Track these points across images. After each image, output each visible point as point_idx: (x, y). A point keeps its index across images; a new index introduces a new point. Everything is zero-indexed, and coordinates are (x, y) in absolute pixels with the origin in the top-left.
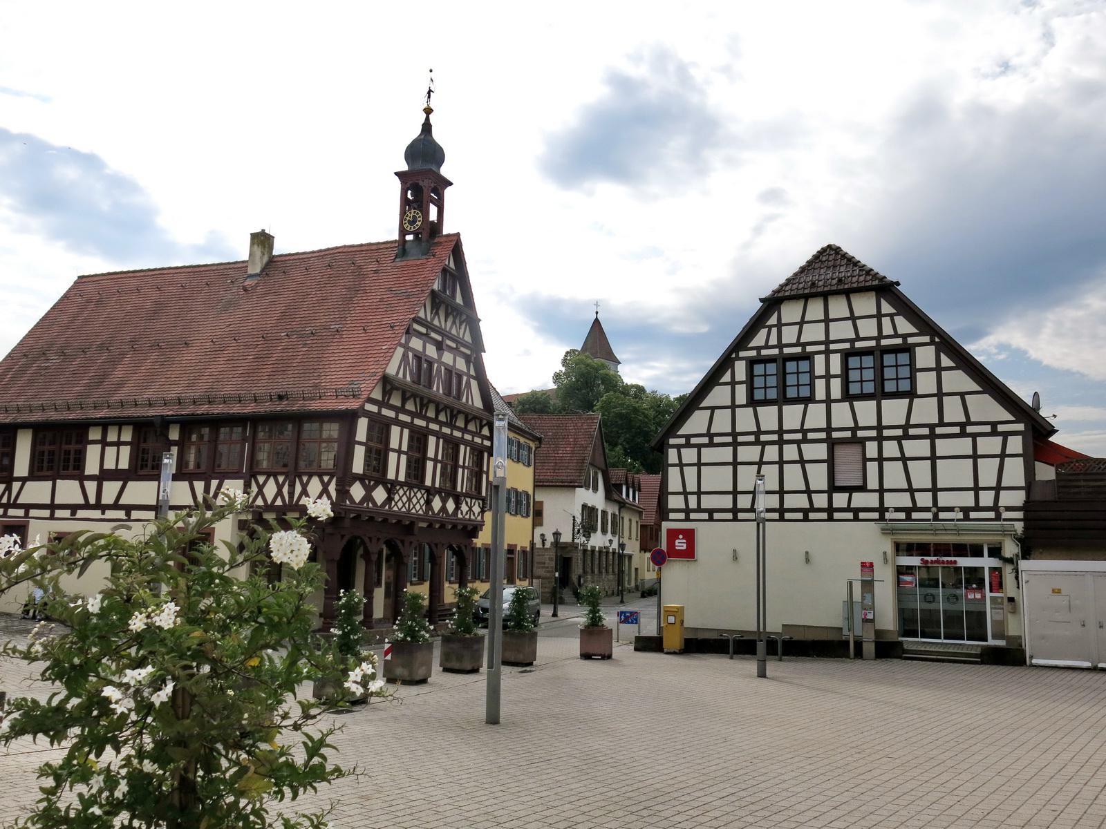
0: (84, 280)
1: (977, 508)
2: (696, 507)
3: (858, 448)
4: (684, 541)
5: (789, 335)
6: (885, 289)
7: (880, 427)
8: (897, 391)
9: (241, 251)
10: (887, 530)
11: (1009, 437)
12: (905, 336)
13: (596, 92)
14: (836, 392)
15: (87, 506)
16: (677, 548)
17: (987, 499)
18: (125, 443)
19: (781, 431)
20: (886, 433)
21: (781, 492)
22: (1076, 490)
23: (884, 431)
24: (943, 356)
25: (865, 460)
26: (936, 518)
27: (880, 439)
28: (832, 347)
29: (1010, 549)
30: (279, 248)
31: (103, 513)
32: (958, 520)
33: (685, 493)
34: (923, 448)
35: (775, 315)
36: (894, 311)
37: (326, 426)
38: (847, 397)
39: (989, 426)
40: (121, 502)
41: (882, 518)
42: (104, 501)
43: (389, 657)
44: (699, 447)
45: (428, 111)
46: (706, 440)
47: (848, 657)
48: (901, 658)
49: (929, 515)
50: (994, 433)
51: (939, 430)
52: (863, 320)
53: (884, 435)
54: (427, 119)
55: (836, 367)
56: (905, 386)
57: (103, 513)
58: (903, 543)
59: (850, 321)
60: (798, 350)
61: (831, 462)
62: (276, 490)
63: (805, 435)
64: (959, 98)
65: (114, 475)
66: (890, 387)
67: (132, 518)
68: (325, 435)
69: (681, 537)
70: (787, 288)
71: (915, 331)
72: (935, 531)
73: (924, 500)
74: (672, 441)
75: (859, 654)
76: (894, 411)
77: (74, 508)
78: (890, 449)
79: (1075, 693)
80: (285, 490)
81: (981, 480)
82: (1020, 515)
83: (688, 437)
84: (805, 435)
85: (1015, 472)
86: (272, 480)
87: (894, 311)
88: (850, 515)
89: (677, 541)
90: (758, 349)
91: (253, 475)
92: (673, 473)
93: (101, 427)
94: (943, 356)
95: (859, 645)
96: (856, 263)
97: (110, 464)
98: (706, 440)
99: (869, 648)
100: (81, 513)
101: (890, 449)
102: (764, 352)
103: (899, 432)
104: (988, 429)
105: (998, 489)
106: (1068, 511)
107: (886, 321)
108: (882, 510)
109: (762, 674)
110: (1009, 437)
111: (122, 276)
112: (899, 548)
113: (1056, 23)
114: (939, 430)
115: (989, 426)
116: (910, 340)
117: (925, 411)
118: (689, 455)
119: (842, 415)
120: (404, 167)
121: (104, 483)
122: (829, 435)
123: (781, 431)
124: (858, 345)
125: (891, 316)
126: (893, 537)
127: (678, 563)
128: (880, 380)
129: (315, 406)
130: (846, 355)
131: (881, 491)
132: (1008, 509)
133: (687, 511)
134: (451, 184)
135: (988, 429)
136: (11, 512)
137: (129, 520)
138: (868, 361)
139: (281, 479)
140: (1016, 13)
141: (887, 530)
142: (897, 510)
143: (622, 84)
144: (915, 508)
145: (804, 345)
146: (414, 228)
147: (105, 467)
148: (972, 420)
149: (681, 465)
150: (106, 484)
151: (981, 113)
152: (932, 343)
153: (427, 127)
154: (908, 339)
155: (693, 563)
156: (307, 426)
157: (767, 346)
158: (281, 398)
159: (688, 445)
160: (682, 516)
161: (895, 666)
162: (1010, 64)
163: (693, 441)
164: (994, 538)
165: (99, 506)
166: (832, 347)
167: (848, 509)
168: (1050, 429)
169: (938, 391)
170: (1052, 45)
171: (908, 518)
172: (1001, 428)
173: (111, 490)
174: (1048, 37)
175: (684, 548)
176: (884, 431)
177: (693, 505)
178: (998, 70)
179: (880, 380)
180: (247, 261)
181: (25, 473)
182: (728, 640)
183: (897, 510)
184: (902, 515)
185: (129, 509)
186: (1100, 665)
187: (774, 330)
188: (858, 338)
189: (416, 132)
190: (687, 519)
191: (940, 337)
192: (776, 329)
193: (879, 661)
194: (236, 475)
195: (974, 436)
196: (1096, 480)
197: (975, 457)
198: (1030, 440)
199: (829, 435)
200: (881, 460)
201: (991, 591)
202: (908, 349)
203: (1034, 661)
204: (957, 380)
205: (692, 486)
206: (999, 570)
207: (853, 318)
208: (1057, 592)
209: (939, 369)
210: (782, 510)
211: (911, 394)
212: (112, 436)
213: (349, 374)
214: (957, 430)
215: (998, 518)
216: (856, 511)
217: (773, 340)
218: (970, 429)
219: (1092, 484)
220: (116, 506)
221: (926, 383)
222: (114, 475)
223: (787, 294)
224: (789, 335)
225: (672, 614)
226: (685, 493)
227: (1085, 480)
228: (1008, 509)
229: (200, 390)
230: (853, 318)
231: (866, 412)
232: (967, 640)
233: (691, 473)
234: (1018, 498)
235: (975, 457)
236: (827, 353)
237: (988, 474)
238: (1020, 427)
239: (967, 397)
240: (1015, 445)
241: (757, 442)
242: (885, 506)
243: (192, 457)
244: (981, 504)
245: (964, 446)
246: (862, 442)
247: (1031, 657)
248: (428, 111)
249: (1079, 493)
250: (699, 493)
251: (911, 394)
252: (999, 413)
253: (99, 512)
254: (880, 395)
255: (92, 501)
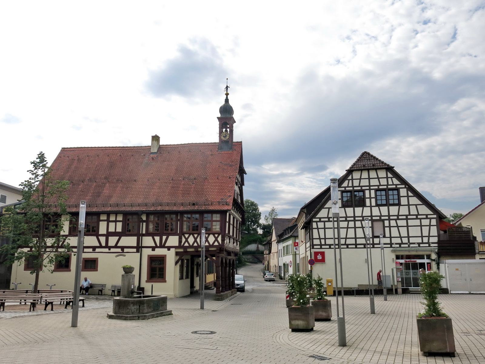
0: (66, 150)
1: (423, 243)
2: (324, 244)
3: (381, 223)
4: (321, 256)
5: (356, 183)
6: (389, 169)
7: (389, 216)
8: (394, 204)
9: (148, 142)
10: (393, 251)
11: (432, 220)
12: (396, 185)
13: (174, 54)
14: (373, 203)
15: (101, 247)
16: (318, 259)
17: (425, 240)
18: (119, 221)
19: (354, 217)
20: (391, 218)
21: (356, 238)
22: (454, 237)
23: (391, 217)
24: (409, 192)
25: (384, 227)
26: (409, 247)
27: (389, 220)
28: (372, 188)
29: (434, 256)
30: (162, 143)
31: (109, 250)
32: (397, 247)
33: (320, 239)
34: (404, 223)
35: (351, 176)
36: (392, 176)
37: (214, 215)
38: (377, 205)
39: (425, 216)
40: (119, 245)
41: (391, 247)
42: (110, 245)
43: (288, 299)
44: (324, 222)
45: (227, 94)
46: (327, 220)
47: (393, 294)
48: (409, 293)
49: (407, 246)
50: (427, 218)
51: (409, 217)
52: (382, 179)
53: (391, 218)
54: (227, 97)
55: (373, 195)
56: (396, 202)
57: (109, 250)
58: (405, 255)
59: (377, 179)
60: (359, 188)
61: (372, 227)
62: (194, 240)
63: (363, 218)
64: (322, 72)
65: (114, 234)
66: (391, 202)
67: (124, 251)
68: (214, 219)
69: (319, 254)
70: (355, 166)
71: (400, 183)
72: (409, 251)
73: (405, 240)
74: (314, 220)
75: (396, 293)
76: (394, 210)
77: (94, 248)
78: (393, 223)
79: (356, 316)
80: (198, 240)
81: (423, 234)
82: (436, 245)
83: (320, 218)
84: (363, 218)
85: (434, 231)
86: (191, 236)
87: (392, 176)
88: (345, 246)
89: (318, 256)
90: (345, 187)
91: (183, 234)
92: (315, 232)
93: (122, 214)
94: (409, 192)
95: (396, 290)
96: (377, 159)
97: (112, 229)
98: (327, 220)
99: (400, 291)
100: (97, 250)
101: (393, 223)
102: (347, 189)
103: (396, 217)
104: (425, 217)
105: (429, 236)
106: (452, 244)
107: (390, 180)
108: (391, 244)
109: (386, 300)
110: (432, 220)
111: (95, 149)
112: (398, 257)
113: (358, 47)
114: (409, 217)
115: (425, 216)
116: (398, 186)
117: (404, 211)
118: (321, 225)
119: (376, 211)
120: (219, 115)
121: (109, 237)
122: (372, 218)
123: (354, 217)
124: (380, 187)
125: (391, 178)
126: (395, 253)
127: (318, 264)
128: (387, 199)
129: (211, 208)
130: (376, 190)
131: (391, 237)
132: (433, 243)
133: (321, 245)
134: (218, 118)
135: (425, 217)
136: (60, 250)
137: (123, 252)
138: (383, 193)
139: (196, 236)
140: (344, 41)
141: (393, 251)
142: (396, 244)
143: (186, 52)
144: (402, 243)
145: (362, 187)
146: (226, 139)
147: (110, 231)
148: (420, 214)
149: (318, 228)
150: (110, 238)
151: (329, 79)
152: (405, 188)
153: (227, 100)
154: (398, 186)
155: (324, 264)
156: (205, 215)
157: (348, 187)
158: (194, 204)
159: (320, 221)
160: (319, 247)
161: (409, 296)
162: (341, 61)
163: (322, 220)
164: (428, 253)
165: (107, 246)
166: (372, 188)
167: (345, 244)
168: (445, 217)
169: (408, 205)
170: (356, 55)
171: (400, 247)
172: (429, 216)
173: (112, 241)
174: (354, 51)
175: (321, 258)
176: (391, 217)
177: (323, 242)
178: (336, 63)
179: (387, 199)
180: (150, 146)
181: (67, 233)
182: (354, 290)
183: (396, 244)
184: (398, 246)
185: (123, 248)
186: (472, 292)
187: (351, 181)
188: (380, 185)
189: (223, 103)
190: (321, 248)
191: (408, 185)
192: (351, 181)
193: (404, 295)
194: (174, 234)
195: (420, 219)
196: (460, 234)
197: (421, 226)
198: (438, 220)
199: (372, 218)
200: (390, 227)
201: (428, 270)
202: (398, 190)
203: (451, 292)
204: (414, 200)
205: (322, 236)
206: (430, 263)
207: (378, 178)
208: (457, 270)
209: (408, 196)
210: (356, 245)
211: (399, 204)
212: (112, 218)
213: (216, 197)
214: (415, 217)
215: (429, 246)
216: (348, 245)
217: (350, 185)
218: (419, 217)
219: (459, 235)
220: (116, 246)
221: (404, 201)
222: (114, 234)
223: (355, 169)
224: (356, 183)
225: (330, 282)
226: (320, 239)
227: (457, 234)
228: (433, 243)
229: (152, 200)
230: (378, 178)
231: (384, 210)
232: (413, 287)
233: (322, 231)
234: (435, 240)
235: (421, 226)
236: (370, 190)
237: (426, 233)
238: (435, 216)
239: (417, 206)
240: (434, 222)
241: (346, 220)
242: (392, 243)
243: (151, 227)
244: (424, 242)
245: (417, 222)
246: (383, 221)
247: (450, 291)
248: (227, 94)
249: (454, 238)
250: (325, 239)
251: (399, 204)
252: (429, 212)
253: (107, 249)
254: (388, 205)
255: (158, 245)
